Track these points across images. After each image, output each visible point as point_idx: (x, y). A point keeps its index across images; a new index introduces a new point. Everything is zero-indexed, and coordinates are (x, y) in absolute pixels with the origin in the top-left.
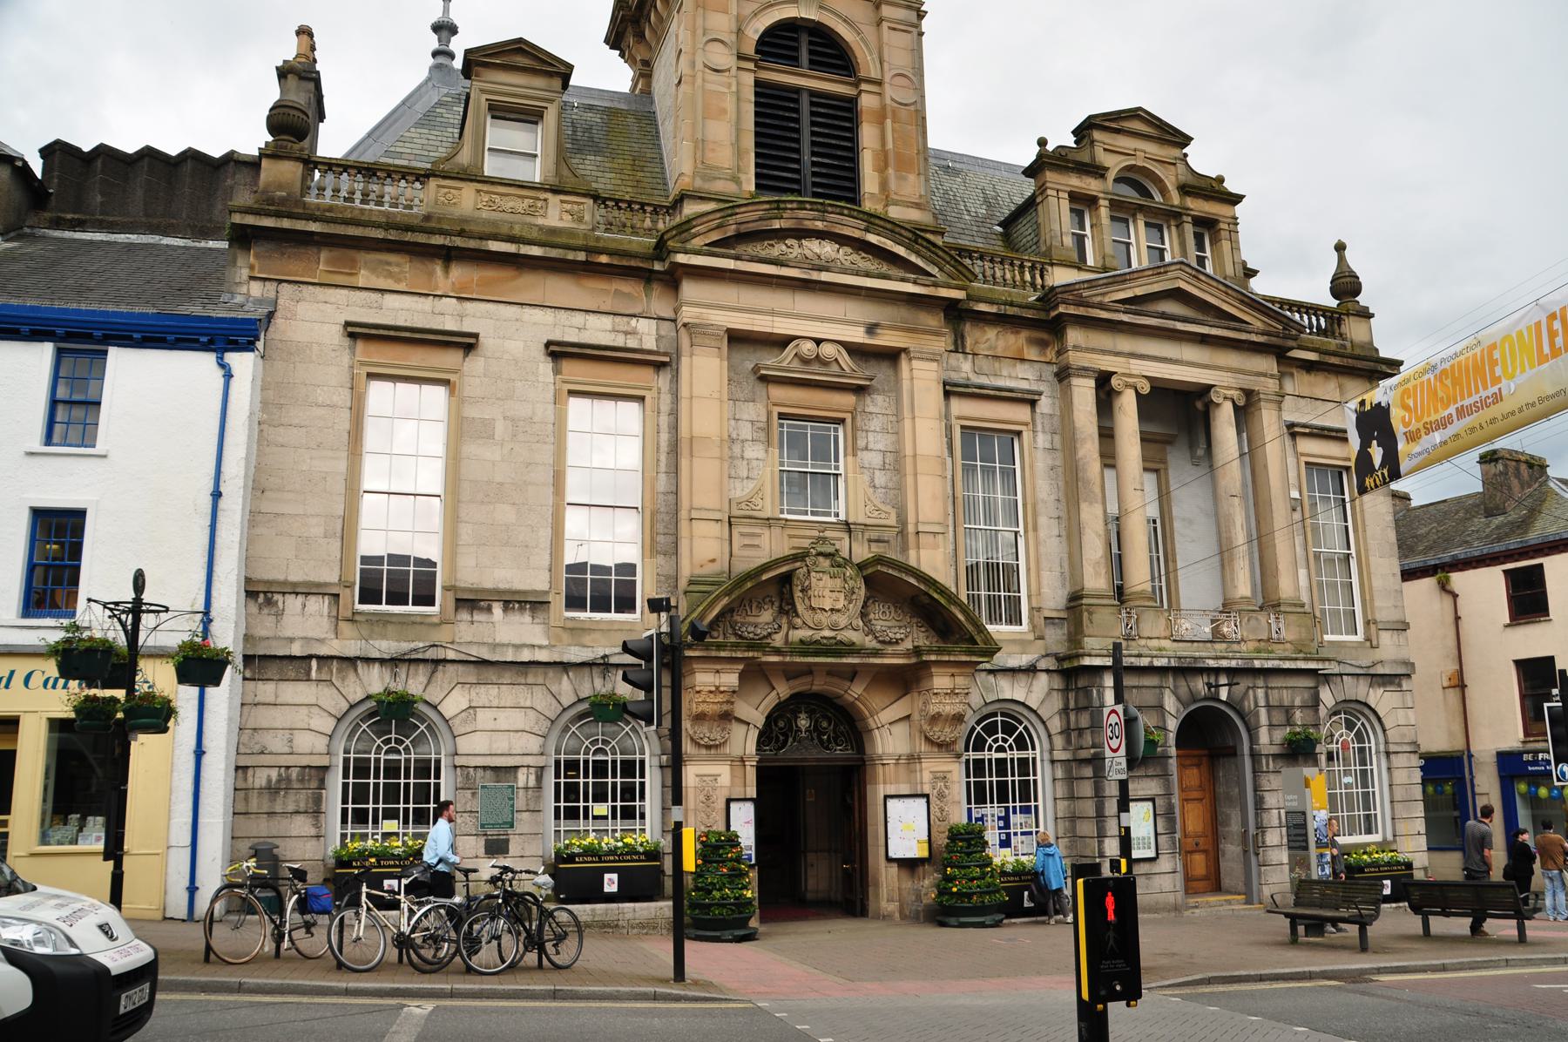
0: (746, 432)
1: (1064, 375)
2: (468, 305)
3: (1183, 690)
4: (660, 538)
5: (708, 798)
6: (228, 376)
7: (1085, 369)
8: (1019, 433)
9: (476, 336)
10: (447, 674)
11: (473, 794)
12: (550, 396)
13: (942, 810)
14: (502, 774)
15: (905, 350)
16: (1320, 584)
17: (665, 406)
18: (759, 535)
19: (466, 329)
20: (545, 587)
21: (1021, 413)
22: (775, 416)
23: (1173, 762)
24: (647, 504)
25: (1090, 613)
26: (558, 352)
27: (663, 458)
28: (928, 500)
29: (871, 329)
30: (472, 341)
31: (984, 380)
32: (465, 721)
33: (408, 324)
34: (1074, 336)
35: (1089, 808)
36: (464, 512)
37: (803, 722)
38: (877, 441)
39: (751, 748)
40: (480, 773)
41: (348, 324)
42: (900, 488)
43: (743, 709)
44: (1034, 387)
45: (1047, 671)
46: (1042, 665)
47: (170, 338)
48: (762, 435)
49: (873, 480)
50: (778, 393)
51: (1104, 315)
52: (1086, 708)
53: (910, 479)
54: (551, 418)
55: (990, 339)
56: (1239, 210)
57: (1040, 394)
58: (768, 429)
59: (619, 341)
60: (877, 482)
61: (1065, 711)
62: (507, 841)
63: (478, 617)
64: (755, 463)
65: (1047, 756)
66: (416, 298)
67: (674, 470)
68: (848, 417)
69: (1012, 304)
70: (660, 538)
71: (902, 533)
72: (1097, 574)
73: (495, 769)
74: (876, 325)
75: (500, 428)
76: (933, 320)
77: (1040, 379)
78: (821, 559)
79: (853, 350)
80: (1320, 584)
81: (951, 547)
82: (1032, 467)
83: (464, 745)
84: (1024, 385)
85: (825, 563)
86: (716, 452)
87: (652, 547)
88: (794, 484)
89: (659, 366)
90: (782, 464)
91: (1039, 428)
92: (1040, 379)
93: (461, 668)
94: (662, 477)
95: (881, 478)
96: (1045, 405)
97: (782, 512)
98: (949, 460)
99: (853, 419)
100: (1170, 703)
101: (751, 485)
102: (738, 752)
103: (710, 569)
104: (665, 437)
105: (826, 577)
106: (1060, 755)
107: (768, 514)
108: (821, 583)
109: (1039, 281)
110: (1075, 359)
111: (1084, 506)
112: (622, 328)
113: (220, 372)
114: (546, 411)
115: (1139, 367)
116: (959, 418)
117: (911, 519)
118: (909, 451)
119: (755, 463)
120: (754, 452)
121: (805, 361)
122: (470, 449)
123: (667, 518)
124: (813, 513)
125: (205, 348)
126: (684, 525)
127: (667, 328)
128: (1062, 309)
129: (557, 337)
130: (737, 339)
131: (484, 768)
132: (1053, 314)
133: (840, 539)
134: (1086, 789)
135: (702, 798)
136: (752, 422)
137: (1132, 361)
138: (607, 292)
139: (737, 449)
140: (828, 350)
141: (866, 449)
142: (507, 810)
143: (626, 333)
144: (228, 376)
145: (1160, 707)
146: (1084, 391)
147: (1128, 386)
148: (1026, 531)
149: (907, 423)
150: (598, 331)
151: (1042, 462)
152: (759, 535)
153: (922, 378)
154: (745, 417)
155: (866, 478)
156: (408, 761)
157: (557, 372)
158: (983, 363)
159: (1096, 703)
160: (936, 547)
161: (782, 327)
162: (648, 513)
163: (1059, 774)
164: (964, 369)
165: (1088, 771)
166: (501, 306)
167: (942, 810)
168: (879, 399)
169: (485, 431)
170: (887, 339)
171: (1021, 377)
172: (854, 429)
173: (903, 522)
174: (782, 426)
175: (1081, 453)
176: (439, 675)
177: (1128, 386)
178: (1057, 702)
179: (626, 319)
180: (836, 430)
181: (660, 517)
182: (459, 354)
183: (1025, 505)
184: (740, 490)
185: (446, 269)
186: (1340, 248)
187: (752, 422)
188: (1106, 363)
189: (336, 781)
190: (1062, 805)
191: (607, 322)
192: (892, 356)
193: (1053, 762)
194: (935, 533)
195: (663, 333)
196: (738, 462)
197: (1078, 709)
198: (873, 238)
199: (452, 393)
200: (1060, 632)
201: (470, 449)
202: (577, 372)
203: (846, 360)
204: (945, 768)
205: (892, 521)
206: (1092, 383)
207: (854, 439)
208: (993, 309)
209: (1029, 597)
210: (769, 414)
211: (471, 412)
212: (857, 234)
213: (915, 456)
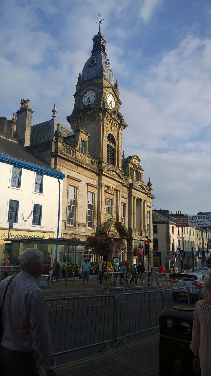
6: (60, 184)
16: (91, 221)
47: (54, 175)
56: (29, 103)
80: (72, 217)
109: (73, 154)
113: (58, 183)
125: (56, 177)
144: (60, 184)
182: (78, 182)
186: (149, 179)
189: (83, 254)
198: (119, 173)
212: (117, 172)
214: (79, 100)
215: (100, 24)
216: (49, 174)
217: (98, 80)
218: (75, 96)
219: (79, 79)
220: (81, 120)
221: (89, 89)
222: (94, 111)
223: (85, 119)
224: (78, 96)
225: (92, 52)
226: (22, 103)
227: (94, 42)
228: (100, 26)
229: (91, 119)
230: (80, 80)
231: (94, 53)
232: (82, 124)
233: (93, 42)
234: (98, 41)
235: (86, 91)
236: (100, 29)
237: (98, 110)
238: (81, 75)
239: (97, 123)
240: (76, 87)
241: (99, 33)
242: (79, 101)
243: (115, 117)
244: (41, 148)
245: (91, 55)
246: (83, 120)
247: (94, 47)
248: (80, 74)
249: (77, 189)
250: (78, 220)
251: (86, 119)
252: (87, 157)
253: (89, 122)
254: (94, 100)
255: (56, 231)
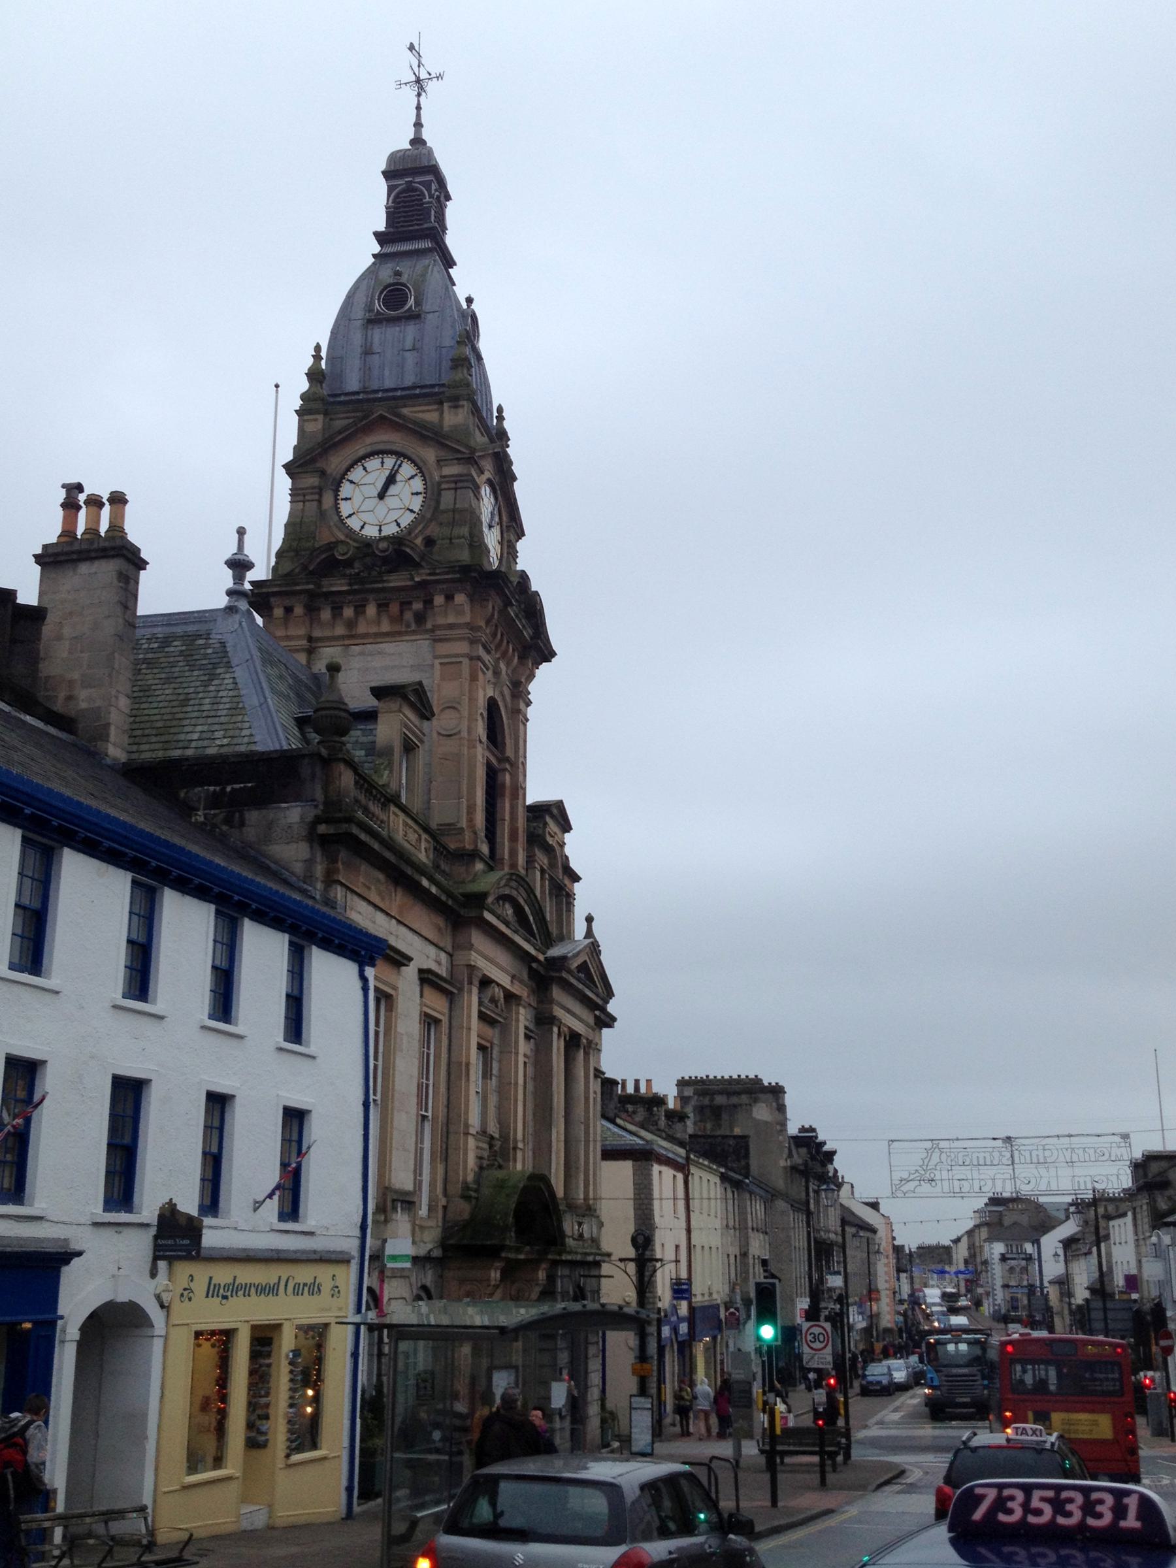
214: (320, 495)
215: (419, 95)
216: (350, 947)
217: (435, 407)
218: (290, 469)
219: (314, 375)
220: (337, 611)
221: (381, 447)
222: (429, 578)
223: (364, 606)
224: (314, 468)
225: (380, 237)
226: (70, 507)
227: (390, 189)
228: (419, 108)
229: (402, 612)
230: (321, 383)
231: (390, 249)
232: (340, 630)
233: (382, 186)
234: (416, 190)
235: (361, 452)
236: (418, 125)
237: (458, 576)
238: (324, 354)
239: (440, 640)
240: (296, 418)
241: (418, 141)
242: (320, 502)
243: (517, 616)
244: (237, 786)
245: (374, 256)
246: (348, 612)
247: (393, 215)
248: (318, 348)
249: (390, 1008)
250: (393, 1181)
251: (371, 610)
252: (421, 832)
253: (386, 627)
254: (416, 510)
255: (355, 1253)
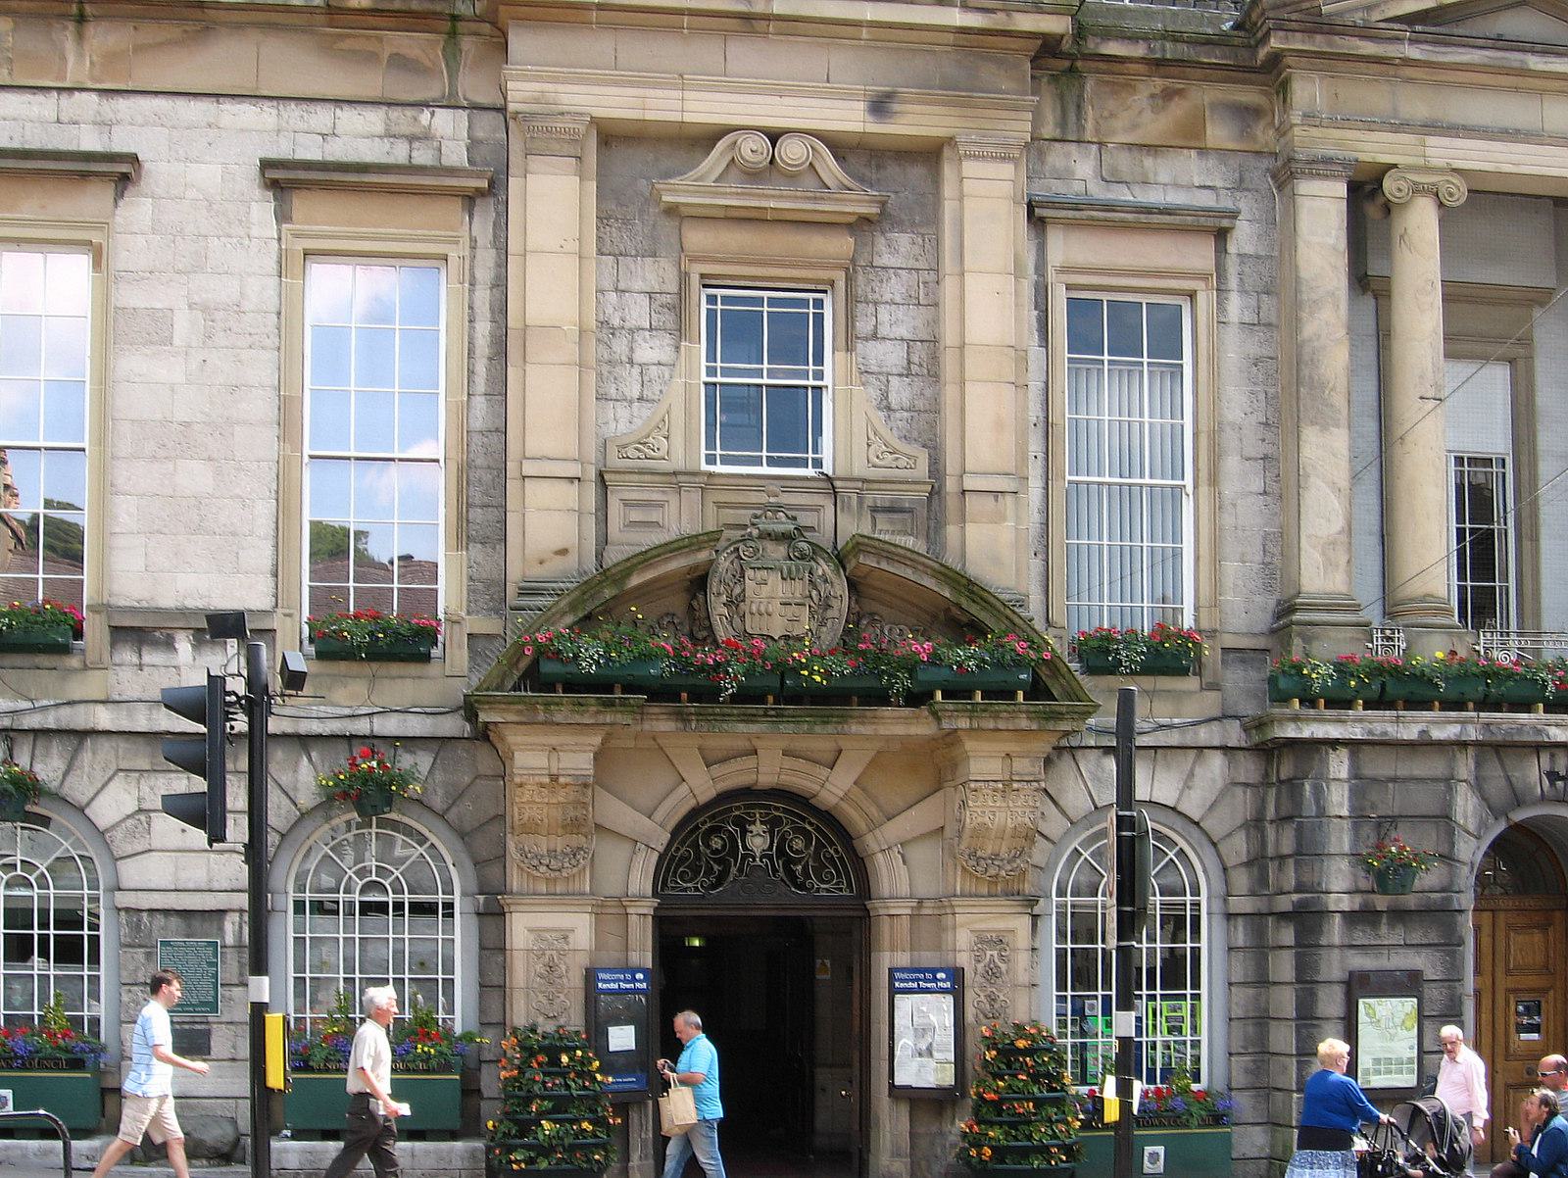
0: (638, 312)
1: (1285, 173)
2: (123, 104)
3: (1496, 786)
4: (477, 514)
5: (551, 968)
7: (1328, 161)
8: (1192, 295)
9: (133, 159)
10: (95, 759)
11: (148, 955)
12: (271, 265)
13: (992, 999)
14: (196, 923)
15: (950, 141)
17: (485, 273)
18: (660, 505)
19: (118, 147)
20: (264, 602)
21: (1199, 255)
22: (695, 280)
23: (1467, 924)
24: (453, 454)
25: (1307, 640)
26: (284, 180)
27: (481, 368)
28: (986, 428)
29: (880, 106)
30: (124, 168)
31: (1123, 194)
32: (132, 834)
33: (16, 145)
34: (1308, 91)
35: (1285, 1001)
36: (122, 475)
37: (758, 841)
38: (898, 321)
39: (642, 880)
40: (160, 920)
41: (266, 165)
42: (935, 408)
43: (615, 812)
44: (1227, 203)
45: (1225, 749)
46: (1204, 735)
48: (668, 319)
49: (885, 396)
50: (698, 238)
51: (1369, 48)
52: (1289, 818)
53: (950, 393)
54: (272, 304)
55: (1137, 114)
57: (1234, 215)
58: (679, 307)
59: (399, 153)
60: (894, 400)
61: (1255, 824)
62: (207, 1034)
63: (150, 657)
64: (654, 371)
65: (1217, 906)
66: (27, 97)
67: (499, 391)
68: (840, 278)
69: (1175, 37)
70: (477, 514)
71: (936, 493)
72: (1330, 564)
73: (186, 914)
74: (889, 96)
75: (184, 326)
76: (1009, 80)
77: (1240, 186)
78: (770, 546)
79: (840, 146)
81: (1035, 518)
82: (1212, 359)
83: (132, 873)
84: (1206, 200)
85: (777, 552)
86: (571, 351)
87: (464, 534)
88: (734, 415)
89: (470, 200)
90: (711, 371)
91: (1233, 282)
92: (1240, 186)
93: (123, 744)
94: (480, 402)
95: (901, 392)
96: (1244, 237)
97: (711, 460)
98: (1036, 353)
99: (849, 280)
100: (1466, 806)
101: (643, 411)
102: (612, 886)
103: (556, 566)
104: (484, 328)
105: (774, 579)
106: (1242, 904)
107: (678, 462)
108: (765, 590)
110: (1308, 140)
111: (1310, 436)
112: (405, 129)
114: (262, 290)
115: (1443, 151)
116: (1065, 270)
117: (951, 466)
118: (949, 337)
119: (654, 371)
120: (652, 350)
121: (753, 175)
122: (131, 364)
123: (487, 477)
124: (772, 462)
126: (512, 486)
127: (487, 123)
128: (1275, 43)
129: (282, 150)
130: (612, 137)
131: (166, 912)
132: (1262, 53)
133: (816, 509)
134: (1284, 967)
135: (540, 968)
136: (650, 294)
137: (1431, 140)
138: (372, 58)
139: (620, 346)
140: (793, 151)
141: (875, 336)
142: (206, 984)
143: (411, 139)
145: (1444, 819)
146: (1322, 209)
147: (1418, 190)
148: (1196, 487)
149: (949, 285)
150: (358, 136)
151: (1236, 349)
152: (660, 505)
153: (984, 199)
154: (638, 285)
155: (873, 393)
156: (44, 899)
157: (283, 216)
158: (1124, 162)
159: (1310, 808)
160: (999, 518)
161: (702, 108)
162: (453, 467)
163: (1240, 938)
164: (1080, 172)
165: (1288, 936)
166: (181, 102)
167: (992, 999)
168: (903, 240)
169: (157, 331)
170: (914, 122)
171: (1183, 180)
172: (851, 300)
173: (936, 469)
174: (712, 299)
175: (1308, 330)
176: (86, 757)
177: (1418, 190)
178: (1241, 805)
179: (410, 112)
180: (819, 304)
181: (475, 475)
183: (1196, 435)
184: (622, 422)
185: (80, 37)
187: (650, 294)
188: (1374, 147)
190: (1241, 995)
191: (374, 119)
192: (929, 155)
193: (1229, 916)
194: (997, 494)
195: (480, 134)
196: (623, 371)
197: (1282, 820)
199: (97, 264)
200: (1253, 674)
201: (131, 364)
202: (318, 216)
203: (830, 168)
204: (1001, 924)
205: (922, 470)
206: (1341, 189)
207: (850, 319)
208: (1139, 50)
209: (1197, 609)
210: (684, 278)
211: (130, 297)
213: (962, 347)
